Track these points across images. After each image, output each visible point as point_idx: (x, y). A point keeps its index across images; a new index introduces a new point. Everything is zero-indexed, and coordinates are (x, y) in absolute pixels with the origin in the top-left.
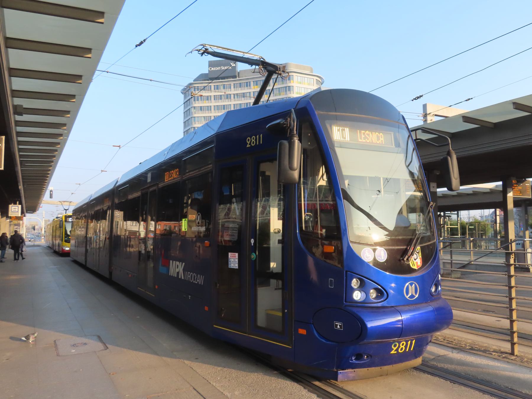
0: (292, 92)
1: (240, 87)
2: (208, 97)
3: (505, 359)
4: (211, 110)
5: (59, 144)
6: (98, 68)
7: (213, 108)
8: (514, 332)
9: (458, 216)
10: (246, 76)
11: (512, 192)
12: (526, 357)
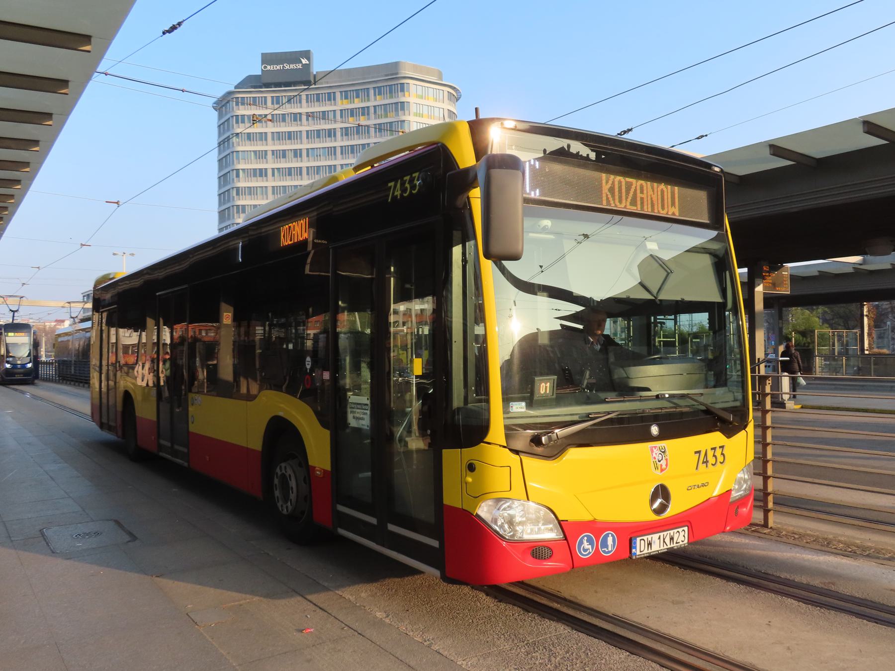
0: (407, 112)
1: (318, 100)
2: (330, 130)
3: (756, 534)
4: (266, 139)
5: (12, 196)
6: (99, 70)
7: (269, 136)
8: (769, 494)
9: (676, 323)
10: (327, 83)
11: (761, 286)
12: (785, 530)
